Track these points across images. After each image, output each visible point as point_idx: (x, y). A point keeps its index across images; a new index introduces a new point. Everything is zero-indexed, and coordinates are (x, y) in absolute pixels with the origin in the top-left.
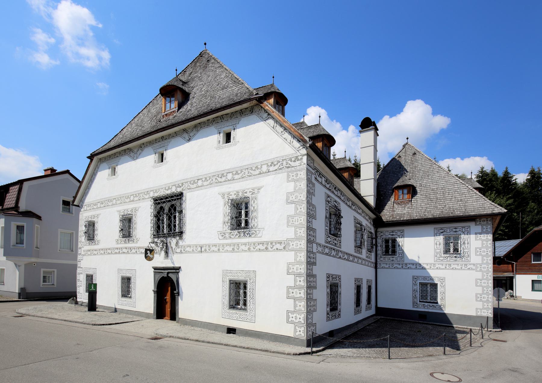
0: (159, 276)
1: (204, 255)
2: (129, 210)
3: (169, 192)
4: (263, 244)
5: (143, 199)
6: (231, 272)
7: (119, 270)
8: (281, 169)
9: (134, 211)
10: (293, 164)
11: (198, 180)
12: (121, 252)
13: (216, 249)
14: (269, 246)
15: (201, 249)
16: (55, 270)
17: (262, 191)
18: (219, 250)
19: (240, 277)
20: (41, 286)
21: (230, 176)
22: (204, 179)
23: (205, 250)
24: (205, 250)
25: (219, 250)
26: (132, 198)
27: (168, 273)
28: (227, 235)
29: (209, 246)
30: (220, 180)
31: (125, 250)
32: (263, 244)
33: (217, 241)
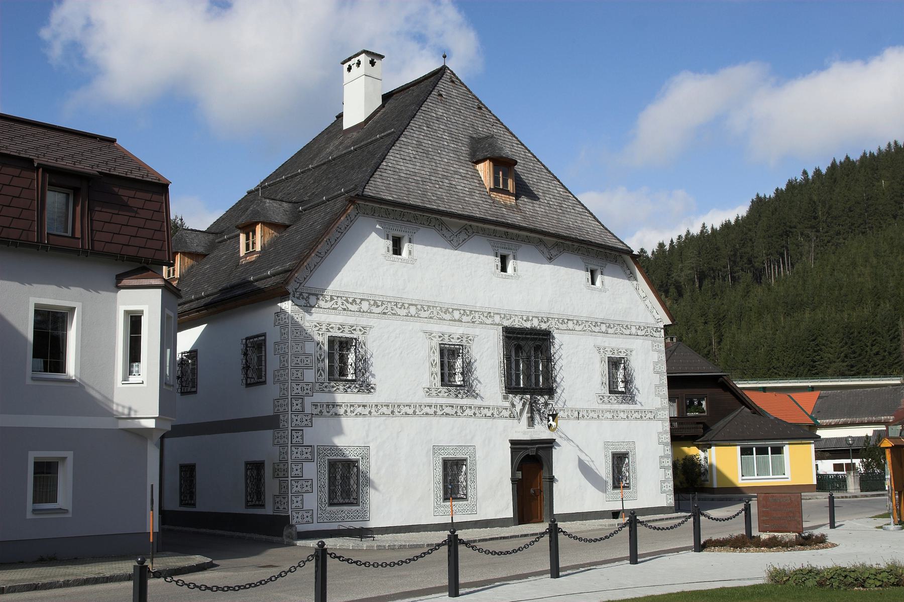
0: (521, 455)
1: (582, 422)
2: (456, 337)
3: (528, 325)
4: (388, 406)
5: (481, 323)
6: (613, 443)
7: (436, 449)
8: (334, 309)
9: (464, 339)
10: (349, 306)
11: (362, 300)
12: (440, 413)
13: (595, 416)
14: (396, 410)
15: (394, 409)
16: (69, 455)
17: (634, 353)
18: (393, 412)
19: (622, 449)
20: (29, 515)
21: (365, 306)
22: (372, 303)
23: (583, 416)
24: (583, 416)
25: (393, 412)
26: (457, 315)
27: (538, 449)
28: (606, 399)
29: (328, 406)
30: (593, 328)
31: (448, 410)
32: (388, 406)
33: (596, 406)
